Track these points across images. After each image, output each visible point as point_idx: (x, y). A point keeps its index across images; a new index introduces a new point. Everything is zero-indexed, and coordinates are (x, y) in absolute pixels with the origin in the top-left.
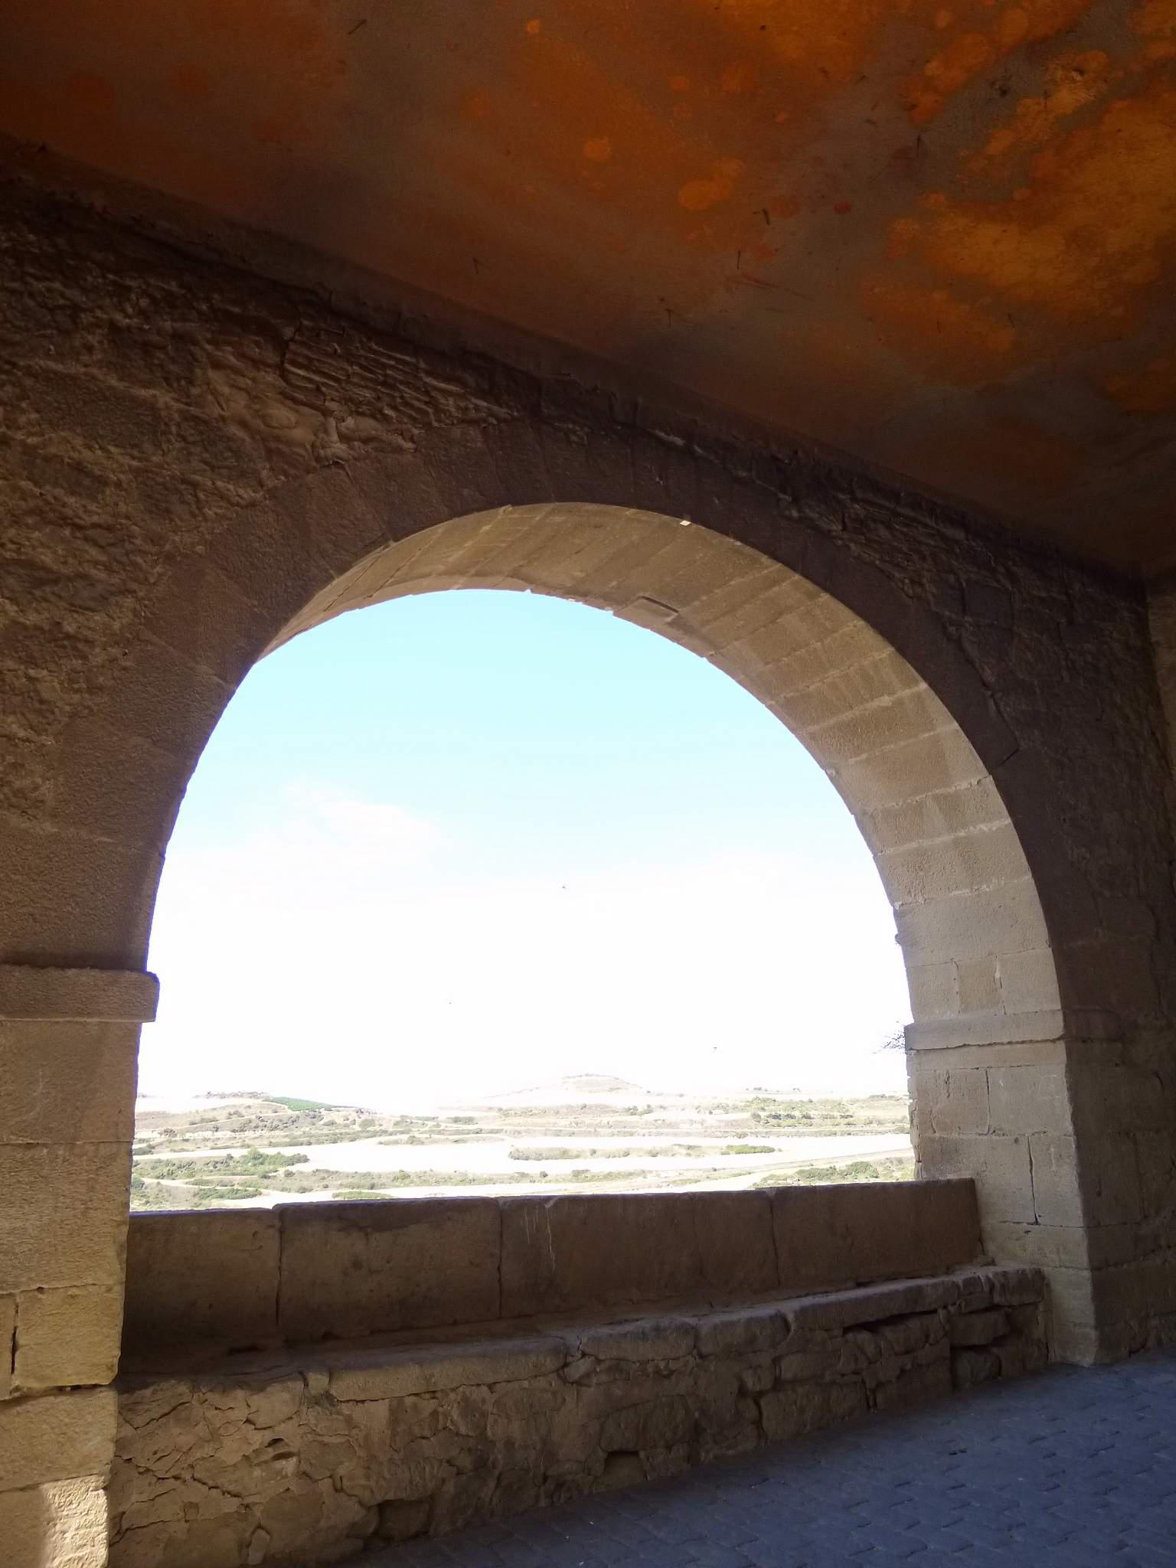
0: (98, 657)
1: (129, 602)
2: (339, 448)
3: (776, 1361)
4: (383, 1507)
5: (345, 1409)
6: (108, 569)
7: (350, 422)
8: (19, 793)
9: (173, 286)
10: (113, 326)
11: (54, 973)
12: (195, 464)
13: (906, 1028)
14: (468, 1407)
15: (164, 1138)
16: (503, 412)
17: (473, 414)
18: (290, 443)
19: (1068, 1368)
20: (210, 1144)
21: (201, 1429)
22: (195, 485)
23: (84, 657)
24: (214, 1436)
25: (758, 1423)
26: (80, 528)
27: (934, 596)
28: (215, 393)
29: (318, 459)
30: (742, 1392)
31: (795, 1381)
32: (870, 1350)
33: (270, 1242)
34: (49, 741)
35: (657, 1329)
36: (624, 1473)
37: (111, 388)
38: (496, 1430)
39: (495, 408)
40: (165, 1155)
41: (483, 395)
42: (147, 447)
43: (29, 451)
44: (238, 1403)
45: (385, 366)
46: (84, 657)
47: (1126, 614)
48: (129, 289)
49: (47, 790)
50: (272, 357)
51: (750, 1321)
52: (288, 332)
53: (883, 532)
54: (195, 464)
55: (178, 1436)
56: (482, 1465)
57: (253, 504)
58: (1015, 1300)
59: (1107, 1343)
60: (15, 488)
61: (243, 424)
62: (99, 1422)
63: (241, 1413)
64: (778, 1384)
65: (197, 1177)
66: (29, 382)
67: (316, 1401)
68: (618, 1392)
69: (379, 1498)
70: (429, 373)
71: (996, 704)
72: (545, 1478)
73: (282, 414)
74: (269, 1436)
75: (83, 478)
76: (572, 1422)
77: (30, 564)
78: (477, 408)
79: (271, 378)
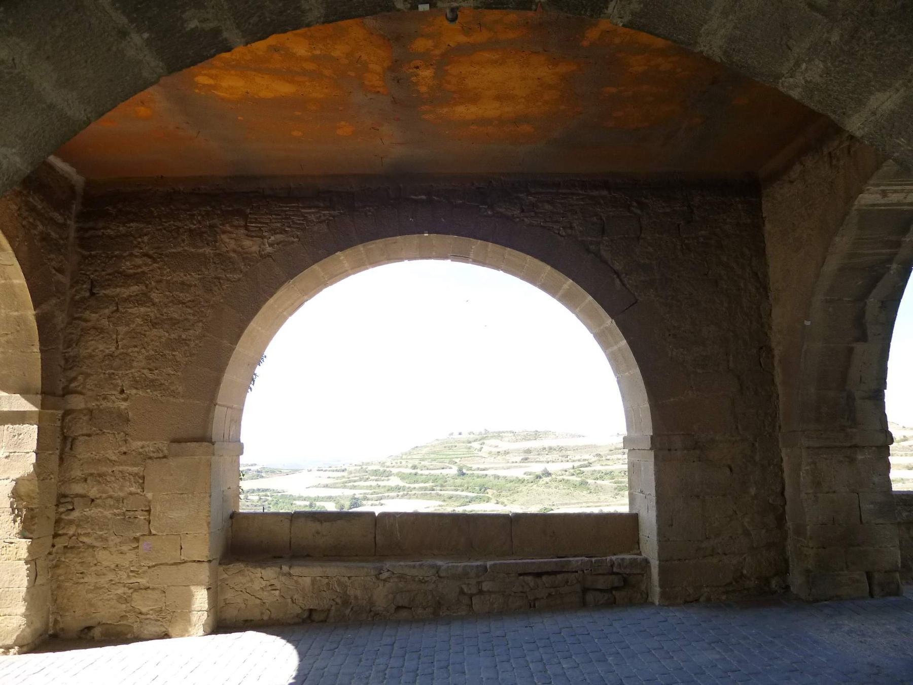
0: (192, 344)
1: (200, 324)
2: (269, 249)
3: (479, 583)
4: (311, 611)
5: (295, 578)
6: (194, 315)
7: (273, 238)
8: (173, 391)
9: (209, 208)
10: (190, 230)
11: (183, 445)
12: (219, 270)
13: (624, 438)
14: (339, 583)
15: (596, 458)
16: (336, 213)
17: (323, 218)
18: (251, 253)
19: (653, 603)
20: (621, 462)
21: (248, 578)
22: (219, 278)
23: (188, 345)
24: (252, 581)
25: (471, 606)
26: (184, 303)
27: (580, 232)
28: (224, 243)
29: (261, 256)
30: (462, 592)
31: (490, 592)
32: (532, 584)
33: (287, 524)
34: (179, 374)
35: (421, 566)
36: (404, 614)
37: (191, 252)
38: (351, 592)
39: (332, 212)
40: (597, 467)
41: (326, 208)
42: (204, 270)
43: (168, 282)
44: (259, 572)
45: (286, 211)
46: (188, 345)
47: (740, 206)
48: (194, 215)
49: (180, 389)
50: (242, 223)
51: (465, 566)
52: (248, 211)
53: (548, 207)
54: (219, 270)
55: (240, 579)
56: (346, 603)
57: (239, 280)
58: (628, 571)
59: (663, 595)
60: (165, 295)
61: (234, 251)
62: (204, 572)
63: (259, 575)
64: (481, 592)
65: (616, 479)
66: (166, 259)
67: (285, 575)
68: (400, 585)
69: (307, 607)
70: (304, 208)
71: (621, 280)
72: (371, 611)
73: (247, 243)
74: (268, 583)
75: (185, 286)
76: (381, 595)
77: (171, 319)
78: (324, 215)
79: (243, 231)
